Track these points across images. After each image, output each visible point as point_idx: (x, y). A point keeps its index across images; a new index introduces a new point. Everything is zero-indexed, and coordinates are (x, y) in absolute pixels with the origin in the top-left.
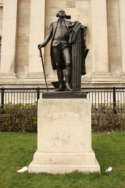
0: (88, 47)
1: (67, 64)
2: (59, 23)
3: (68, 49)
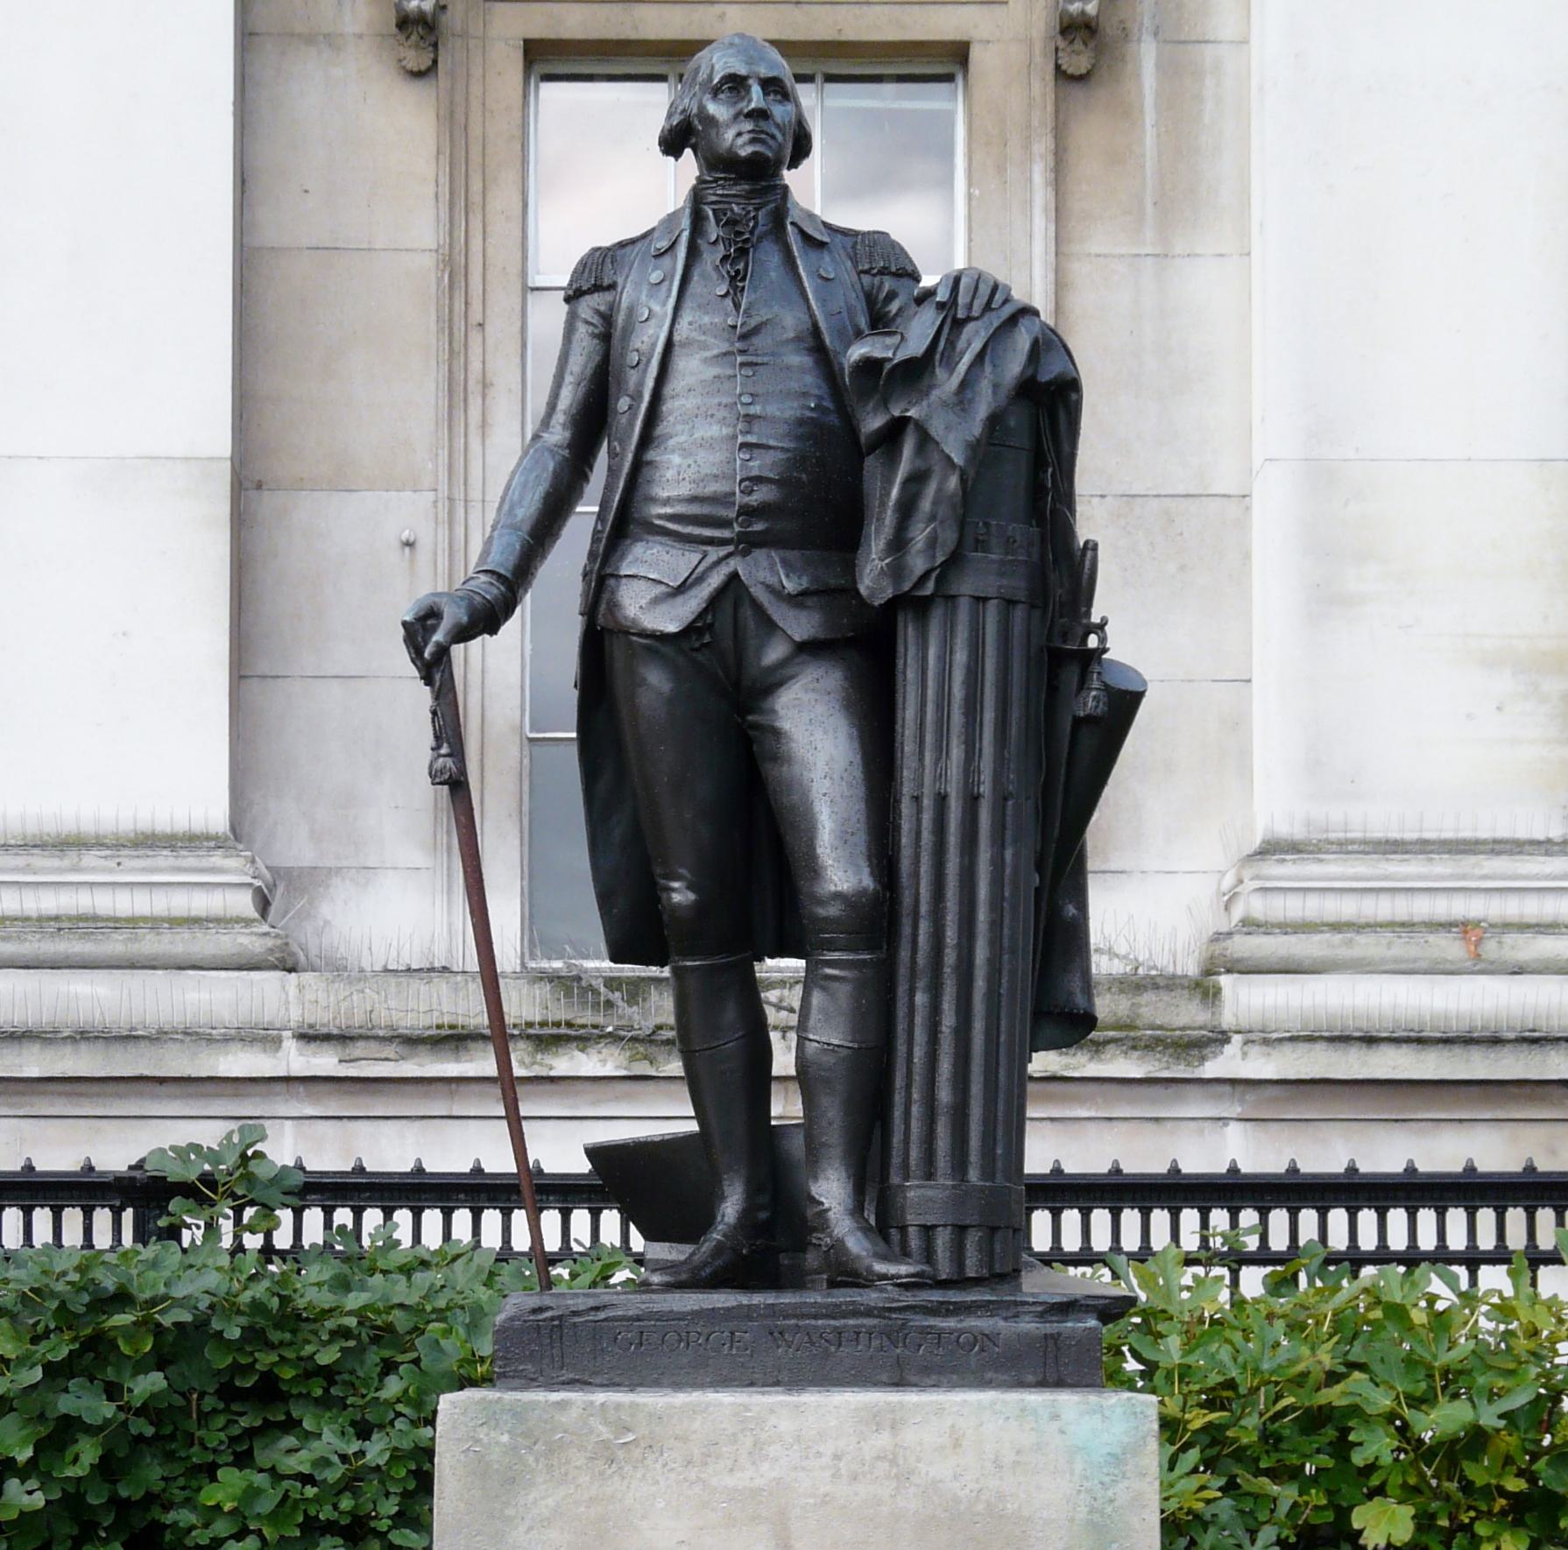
1: (833, 911)
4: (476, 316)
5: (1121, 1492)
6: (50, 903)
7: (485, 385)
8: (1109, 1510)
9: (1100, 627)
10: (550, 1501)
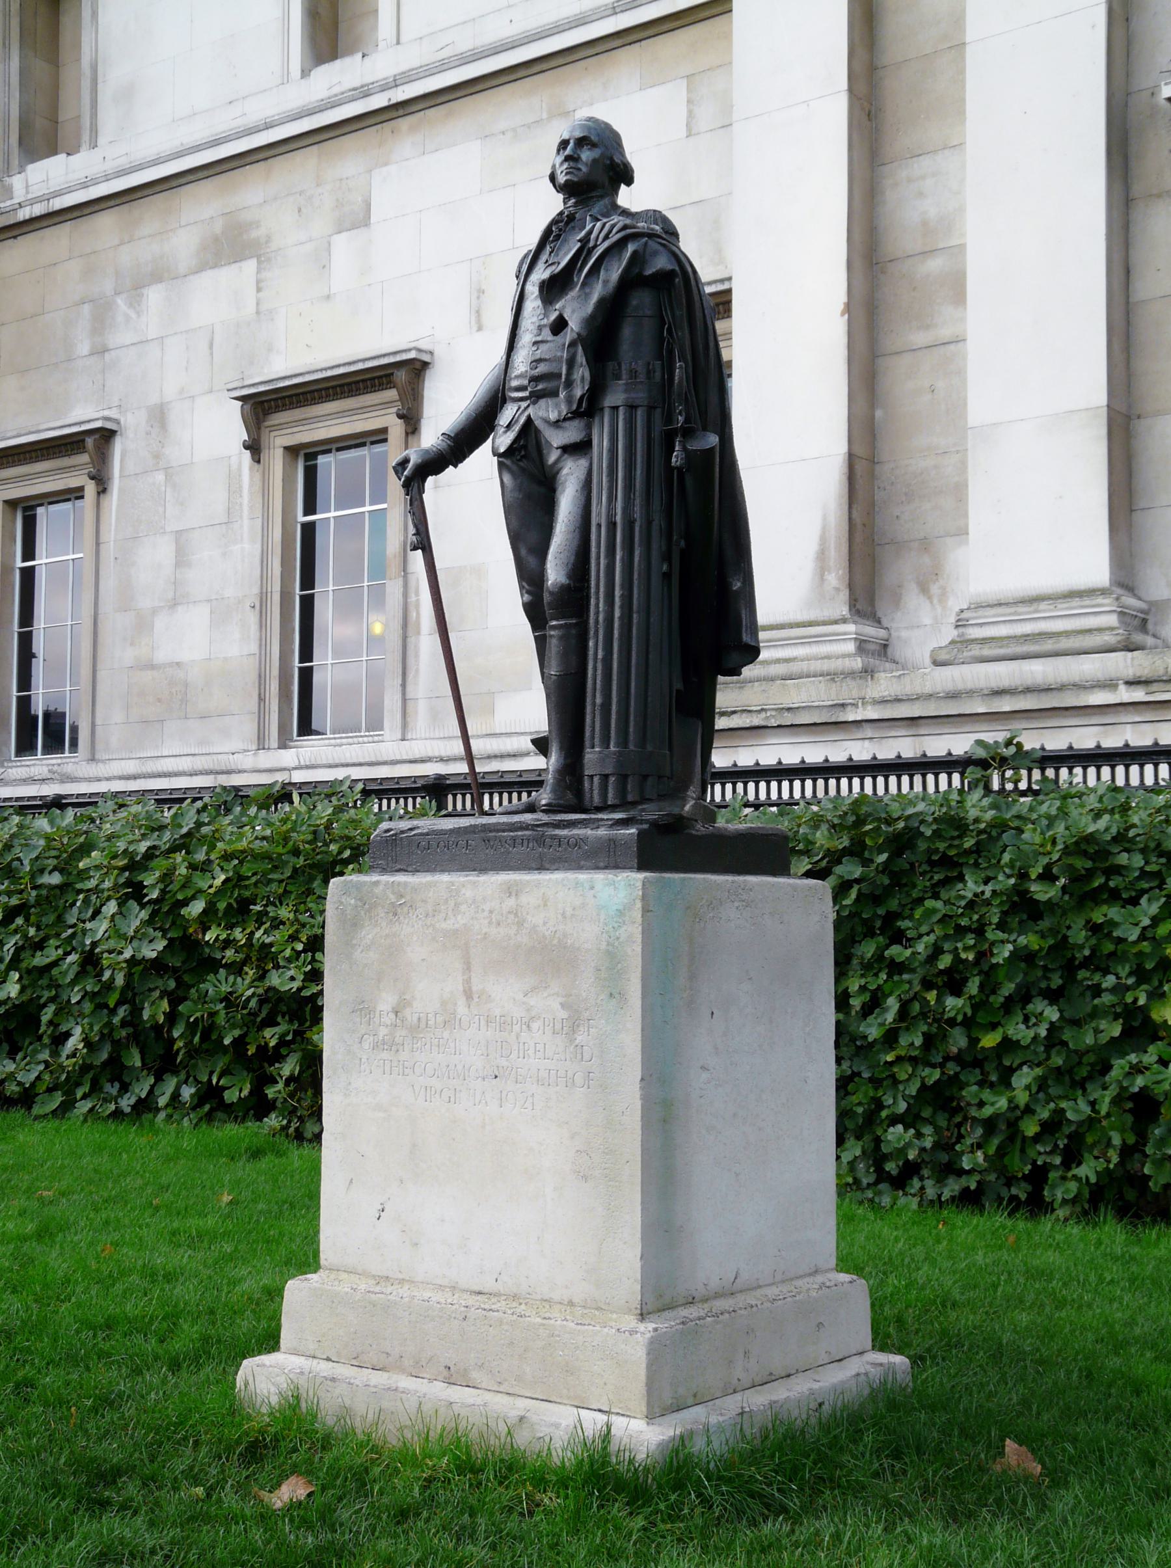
5: (623, 933)
6: (1027, 628)
10: (370, 936)
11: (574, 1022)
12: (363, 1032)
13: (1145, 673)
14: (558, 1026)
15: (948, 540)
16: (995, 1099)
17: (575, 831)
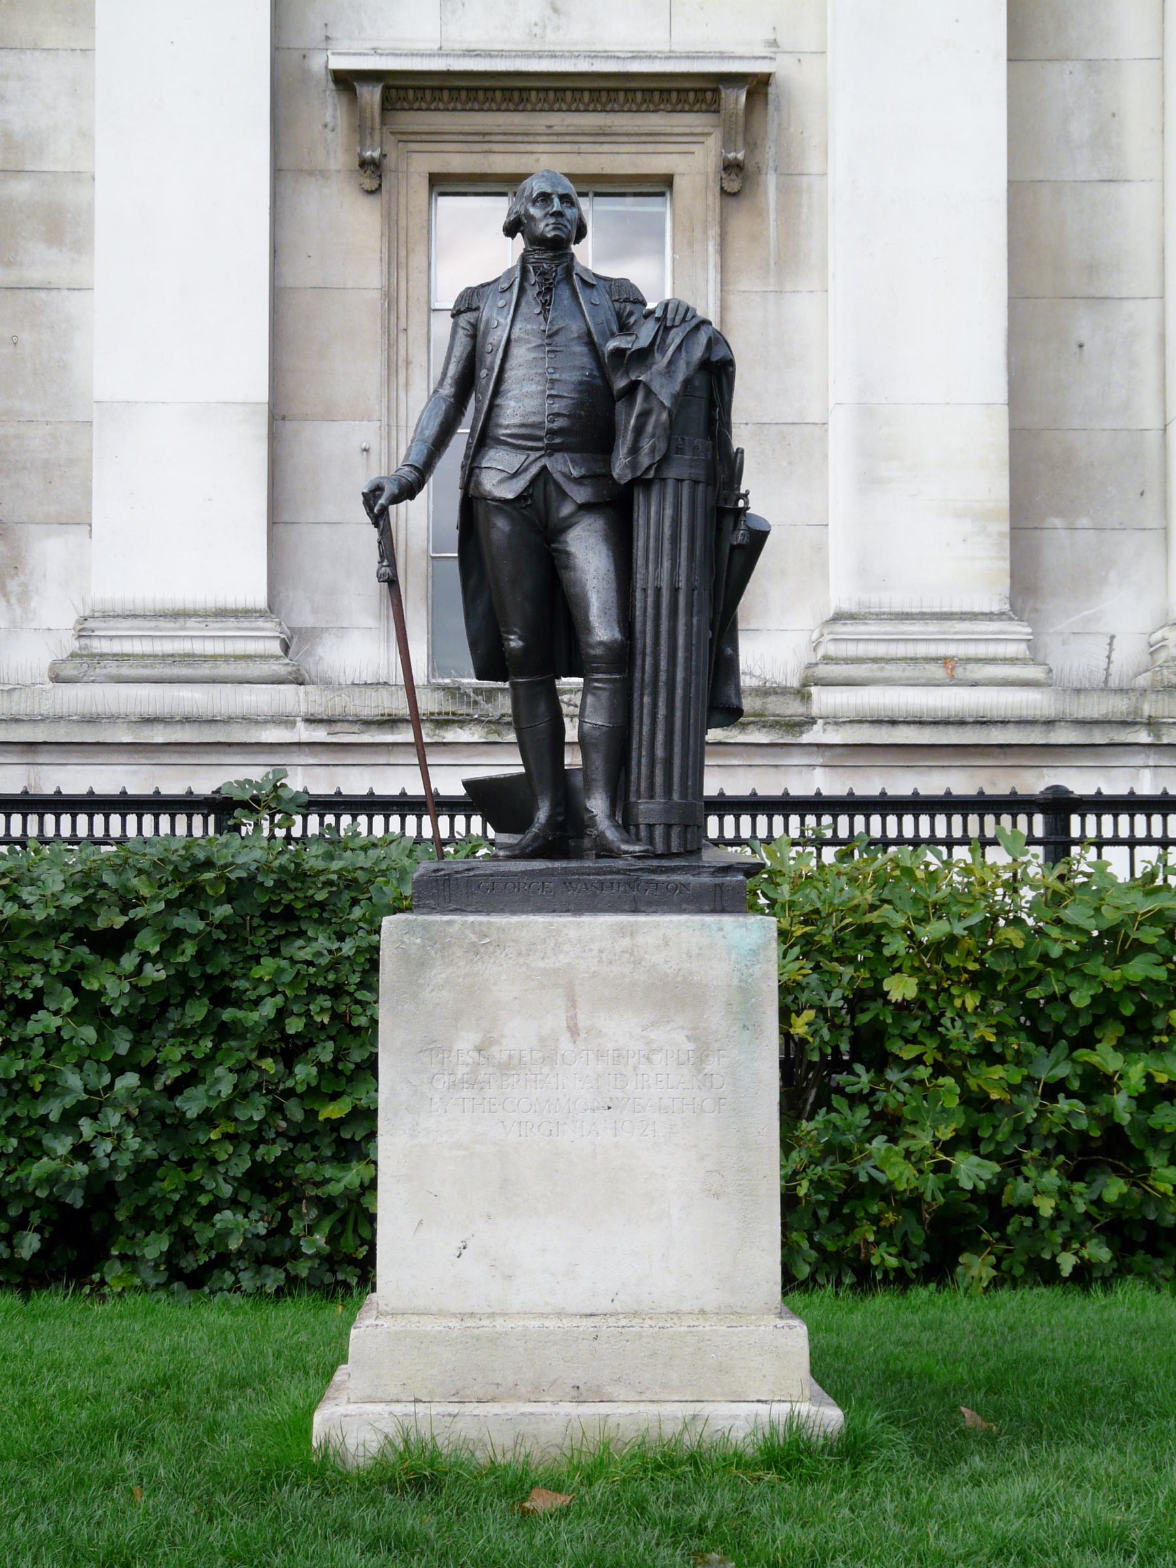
0: (763, 494)
1: (598, 651)
2: (531, 306)
3: (595, 530)
4: (402, 325)
5: (757, 970)
6: (168, 647)
7: (408, 363)
8: (750, 980)
9: (746, 496)
10: (443, 975)
11: (702, 1050)
12: (435, 1071)
13: (319, 711)
14: (683, 1057)
15: (32, 527)
16: (342, 1174)
17: (675, 877)
